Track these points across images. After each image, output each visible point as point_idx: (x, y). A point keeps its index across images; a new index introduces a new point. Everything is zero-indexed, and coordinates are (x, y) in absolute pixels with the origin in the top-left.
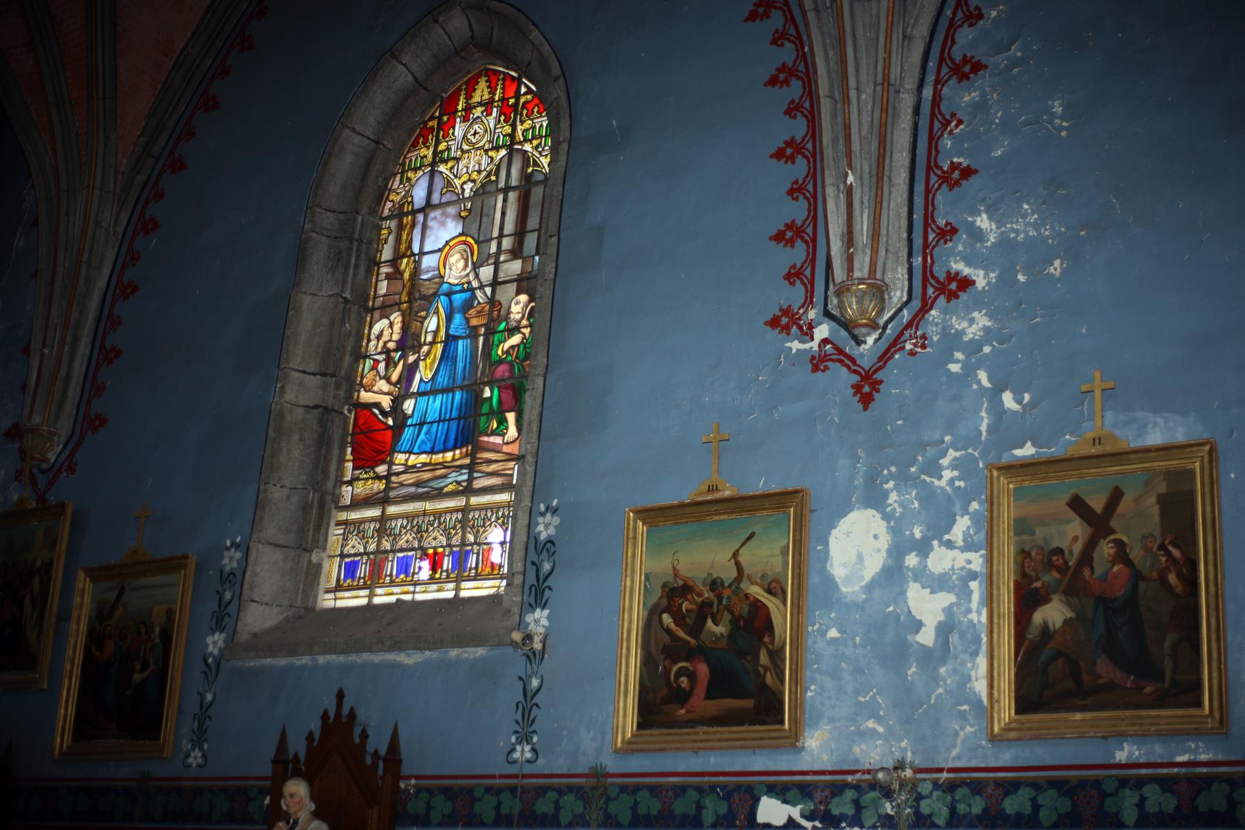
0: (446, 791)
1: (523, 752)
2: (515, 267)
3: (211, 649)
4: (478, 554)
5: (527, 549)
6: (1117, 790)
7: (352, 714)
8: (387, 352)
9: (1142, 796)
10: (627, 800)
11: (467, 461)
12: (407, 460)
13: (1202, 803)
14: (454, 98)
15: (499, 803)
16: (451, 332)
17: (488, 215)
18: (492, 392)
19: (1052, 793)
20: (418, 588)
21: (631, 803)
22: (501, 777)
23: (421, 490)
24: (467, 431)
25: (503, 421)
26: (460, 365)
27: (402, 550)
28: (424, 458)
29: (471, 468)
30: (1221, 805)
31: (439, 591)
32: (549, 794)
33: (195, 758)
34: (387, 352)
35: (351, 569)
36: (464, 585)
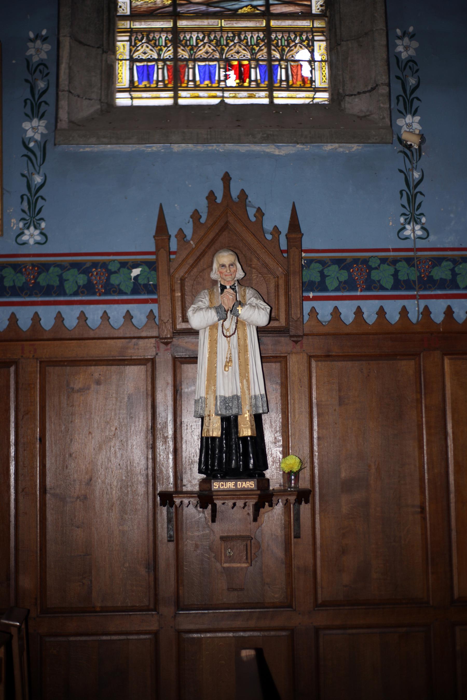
0: (338, 262)
3: (30, 134)
5: (388, 65)
6: (119, 270)
7: (243, 195)
9: (395, 269)
13: (43, 280)
15: (397, 272)
20: (226, 94)
22: (395, 250)
27: (141, 60)
30: (447, 275)
31: (249, 97)
32: (444, 263)
33: (31, 236)
35: (146, 73)
36: (276, 94)
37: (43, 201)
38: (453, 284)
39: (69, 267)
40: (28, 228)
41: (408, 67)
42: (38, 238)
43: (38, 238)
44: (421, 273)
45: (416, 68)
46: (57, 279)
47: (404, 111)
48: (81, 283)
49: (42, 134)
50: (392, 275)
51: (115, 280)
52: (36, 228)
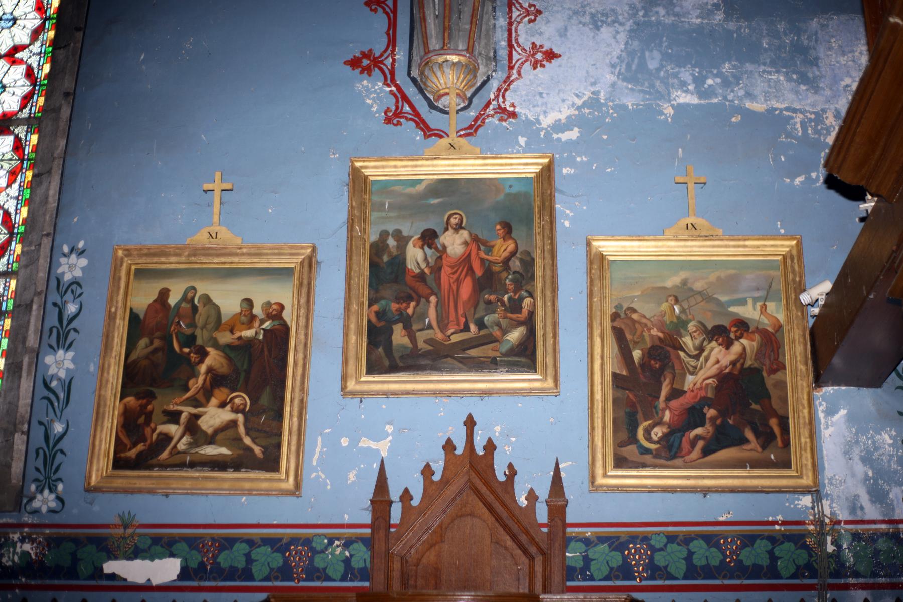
3: (52, 370)
9: (689, 551)
10: (677, 552)
13: (224, 560)
15: (691, 554)
19: (788, 546)
21: (685, 554)
33: (45, 501)
37: (63, 456)
38: (72, 573)
39: (260, 543)
40: (41, 492)
41: (69, 291)
42: (53, 505)
44: (726, 556)
45: (79, 291)
46: (244, 559)
47: (56, 348)
48: (801, 562)
49: (68, 370)
50: (685, 559)
51: (319, 562)
52: (51, 491)
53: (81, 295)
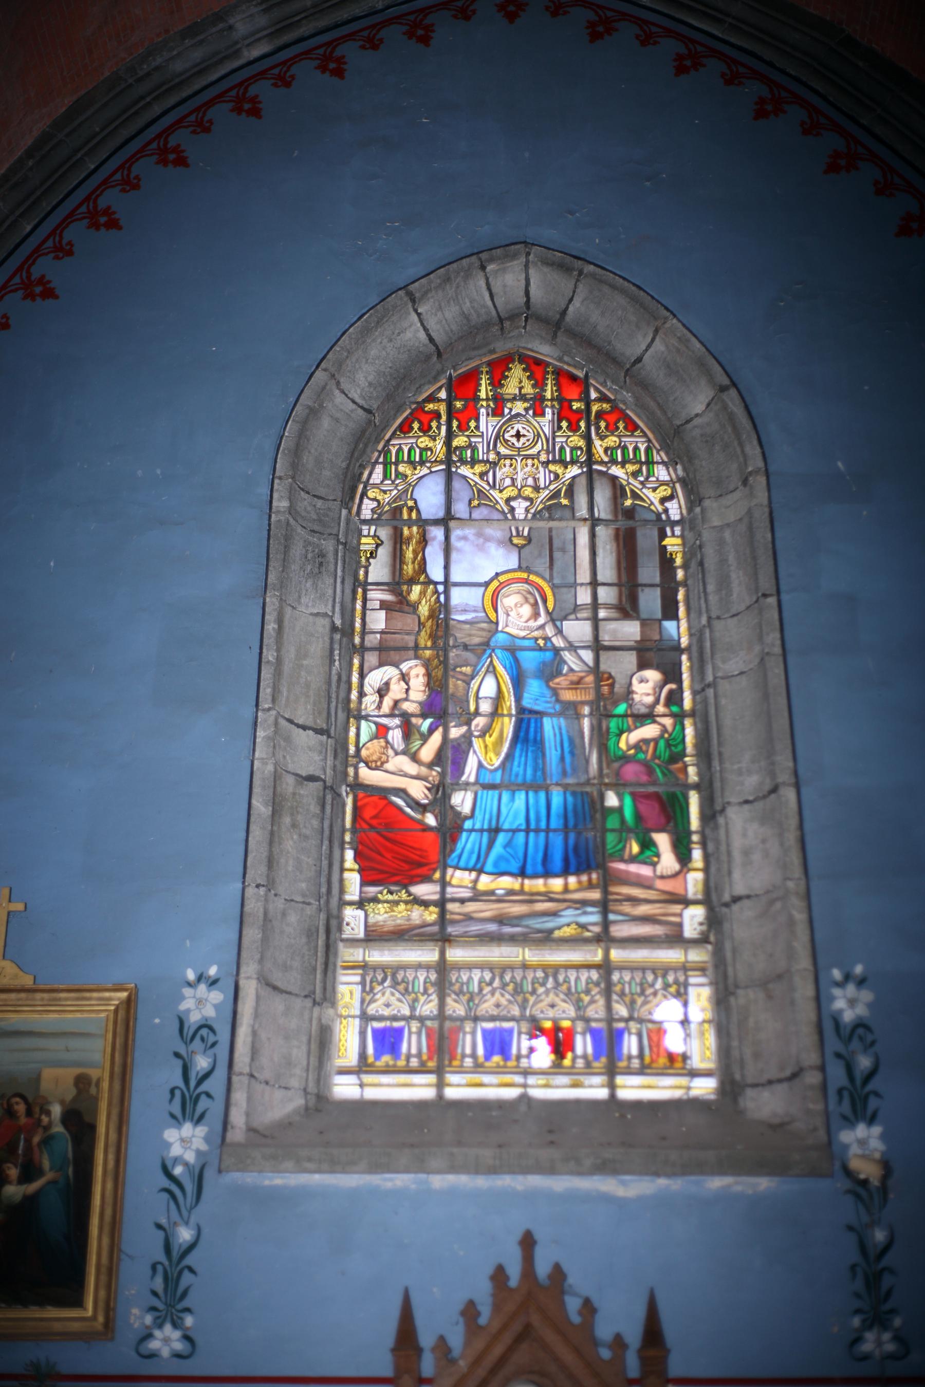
1: (166, 1341)
2: (631, 630)
3: (176, 1150)
4: (639, 1035)
7: (558, 1273)
8: (406, 718)
11: (596, 895)
12: (476, 881)
14: (472, 378)
16: (527, 702)
17: (563, 550)
18: (621, 799)
20: (531, 1080)
23: (507, 930)
24: (584, 847)
25: (647, 844)
26: (552, 755)
28: (507, 882)
29: (604, 906)
33: (166, 1340)
34: (406, 718)
35: (389, 1040)
41: (198, 1037)
42: (178, 1346)
43: (178, 1346)
53: (214, 1044)
